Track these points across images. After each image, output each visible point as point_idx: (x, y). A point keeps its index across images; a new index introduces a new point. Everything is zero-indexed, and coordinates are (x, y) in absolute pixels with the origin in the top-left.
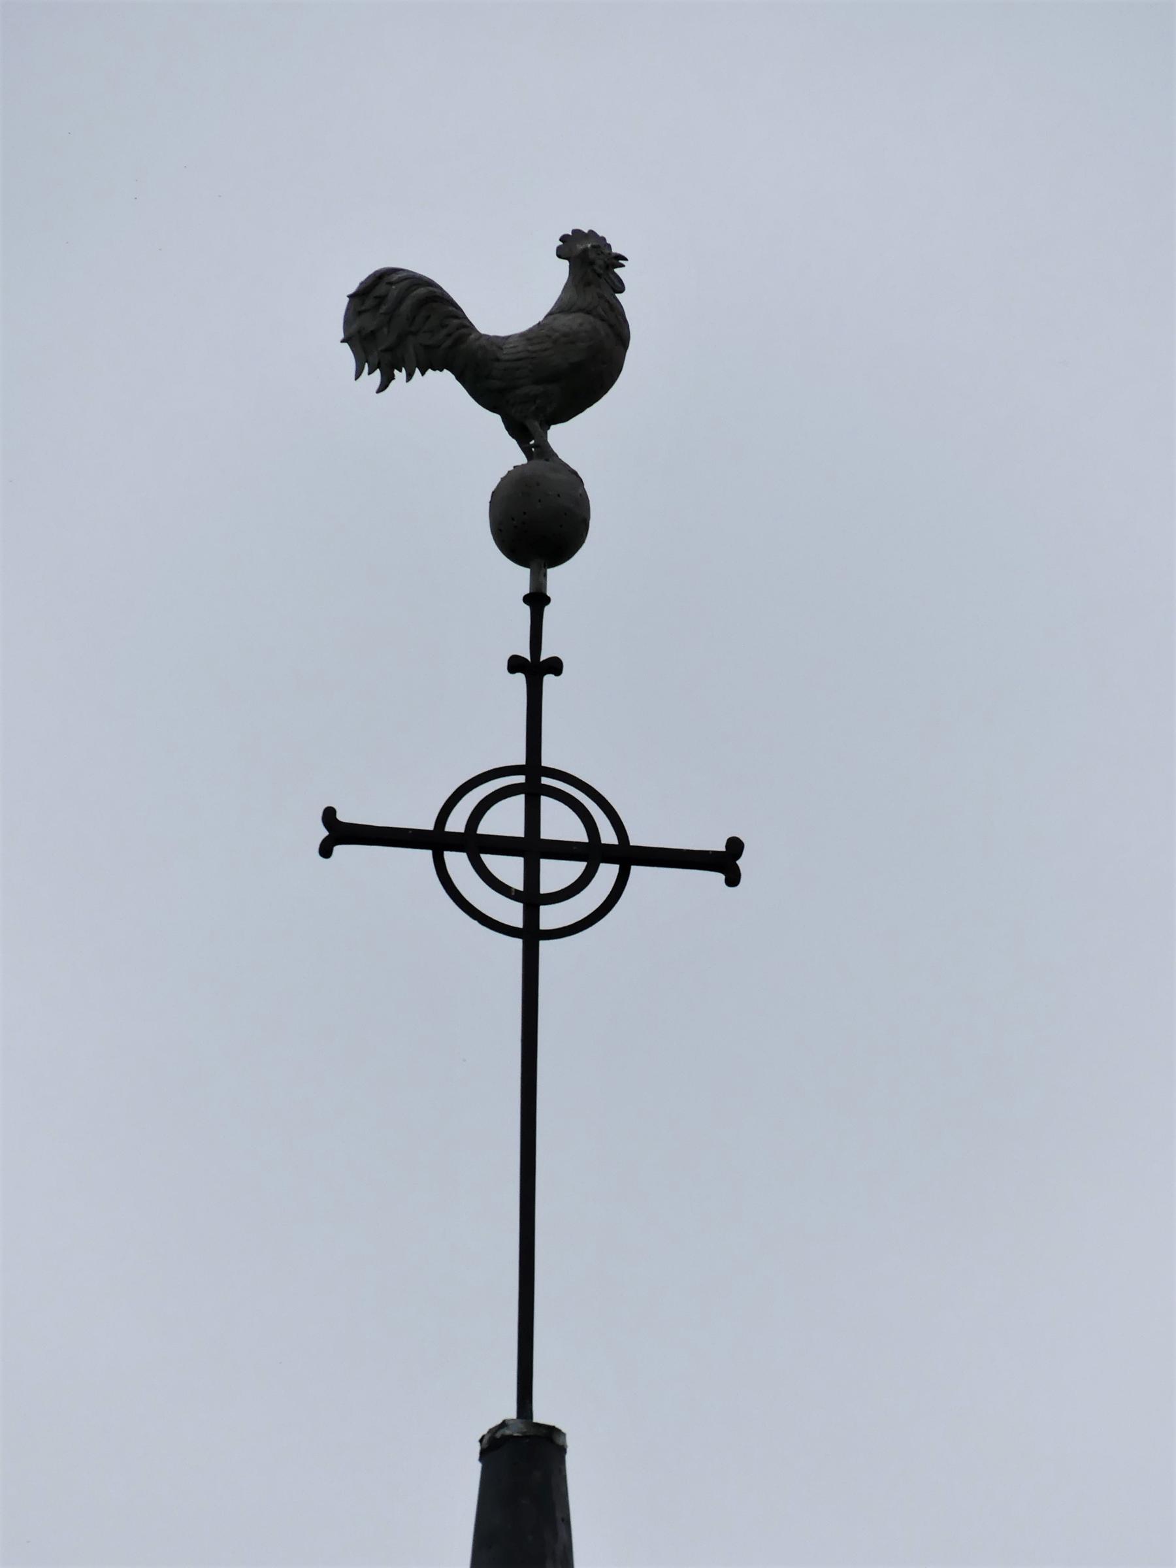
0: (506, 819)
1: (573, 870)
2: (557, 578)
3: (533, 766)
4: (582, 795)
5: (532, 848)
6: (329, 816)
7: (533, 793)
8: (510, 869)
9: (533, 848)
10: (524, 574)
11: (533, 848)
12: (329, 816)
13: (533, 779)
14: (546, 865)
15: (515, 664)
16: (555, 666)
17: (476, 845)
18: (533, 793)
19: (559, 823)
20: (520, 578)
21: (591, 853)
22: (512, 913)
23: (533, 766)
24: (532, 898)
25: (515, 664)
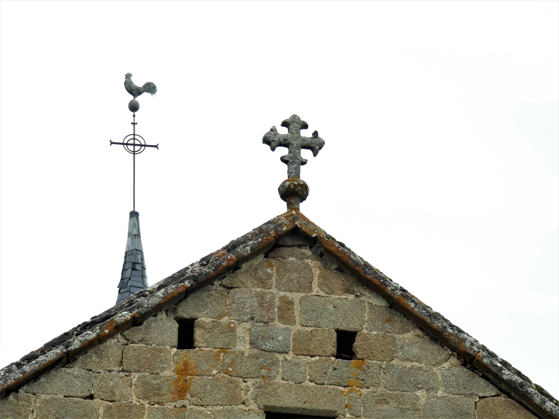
0: (137, 148)
1: (129, 142)
2: (136, 113)
3: (134, 154)
4: (129, 151)
5: (134, 145)
6: (110, 141)
7: (134, 151)
8: (137, 142)
9: (134, 145)
10: (132, 113)
11: (134, 145)
12: (110, 141)
13: (134, 153)
14: (136, 147)
15: (132, 123)
16: (136, 123)
17: (141, 145)
18: (134, 151)
19: (131, 148)
20: (132, 113)
21: (127, 144)
22: (136, 137)
23: (134, 154)
24: (134, 139)
25: (132, 123)
